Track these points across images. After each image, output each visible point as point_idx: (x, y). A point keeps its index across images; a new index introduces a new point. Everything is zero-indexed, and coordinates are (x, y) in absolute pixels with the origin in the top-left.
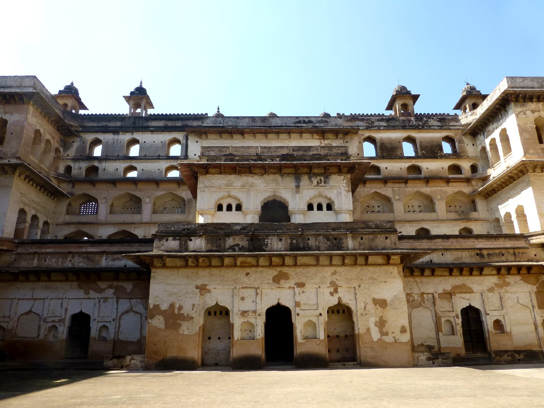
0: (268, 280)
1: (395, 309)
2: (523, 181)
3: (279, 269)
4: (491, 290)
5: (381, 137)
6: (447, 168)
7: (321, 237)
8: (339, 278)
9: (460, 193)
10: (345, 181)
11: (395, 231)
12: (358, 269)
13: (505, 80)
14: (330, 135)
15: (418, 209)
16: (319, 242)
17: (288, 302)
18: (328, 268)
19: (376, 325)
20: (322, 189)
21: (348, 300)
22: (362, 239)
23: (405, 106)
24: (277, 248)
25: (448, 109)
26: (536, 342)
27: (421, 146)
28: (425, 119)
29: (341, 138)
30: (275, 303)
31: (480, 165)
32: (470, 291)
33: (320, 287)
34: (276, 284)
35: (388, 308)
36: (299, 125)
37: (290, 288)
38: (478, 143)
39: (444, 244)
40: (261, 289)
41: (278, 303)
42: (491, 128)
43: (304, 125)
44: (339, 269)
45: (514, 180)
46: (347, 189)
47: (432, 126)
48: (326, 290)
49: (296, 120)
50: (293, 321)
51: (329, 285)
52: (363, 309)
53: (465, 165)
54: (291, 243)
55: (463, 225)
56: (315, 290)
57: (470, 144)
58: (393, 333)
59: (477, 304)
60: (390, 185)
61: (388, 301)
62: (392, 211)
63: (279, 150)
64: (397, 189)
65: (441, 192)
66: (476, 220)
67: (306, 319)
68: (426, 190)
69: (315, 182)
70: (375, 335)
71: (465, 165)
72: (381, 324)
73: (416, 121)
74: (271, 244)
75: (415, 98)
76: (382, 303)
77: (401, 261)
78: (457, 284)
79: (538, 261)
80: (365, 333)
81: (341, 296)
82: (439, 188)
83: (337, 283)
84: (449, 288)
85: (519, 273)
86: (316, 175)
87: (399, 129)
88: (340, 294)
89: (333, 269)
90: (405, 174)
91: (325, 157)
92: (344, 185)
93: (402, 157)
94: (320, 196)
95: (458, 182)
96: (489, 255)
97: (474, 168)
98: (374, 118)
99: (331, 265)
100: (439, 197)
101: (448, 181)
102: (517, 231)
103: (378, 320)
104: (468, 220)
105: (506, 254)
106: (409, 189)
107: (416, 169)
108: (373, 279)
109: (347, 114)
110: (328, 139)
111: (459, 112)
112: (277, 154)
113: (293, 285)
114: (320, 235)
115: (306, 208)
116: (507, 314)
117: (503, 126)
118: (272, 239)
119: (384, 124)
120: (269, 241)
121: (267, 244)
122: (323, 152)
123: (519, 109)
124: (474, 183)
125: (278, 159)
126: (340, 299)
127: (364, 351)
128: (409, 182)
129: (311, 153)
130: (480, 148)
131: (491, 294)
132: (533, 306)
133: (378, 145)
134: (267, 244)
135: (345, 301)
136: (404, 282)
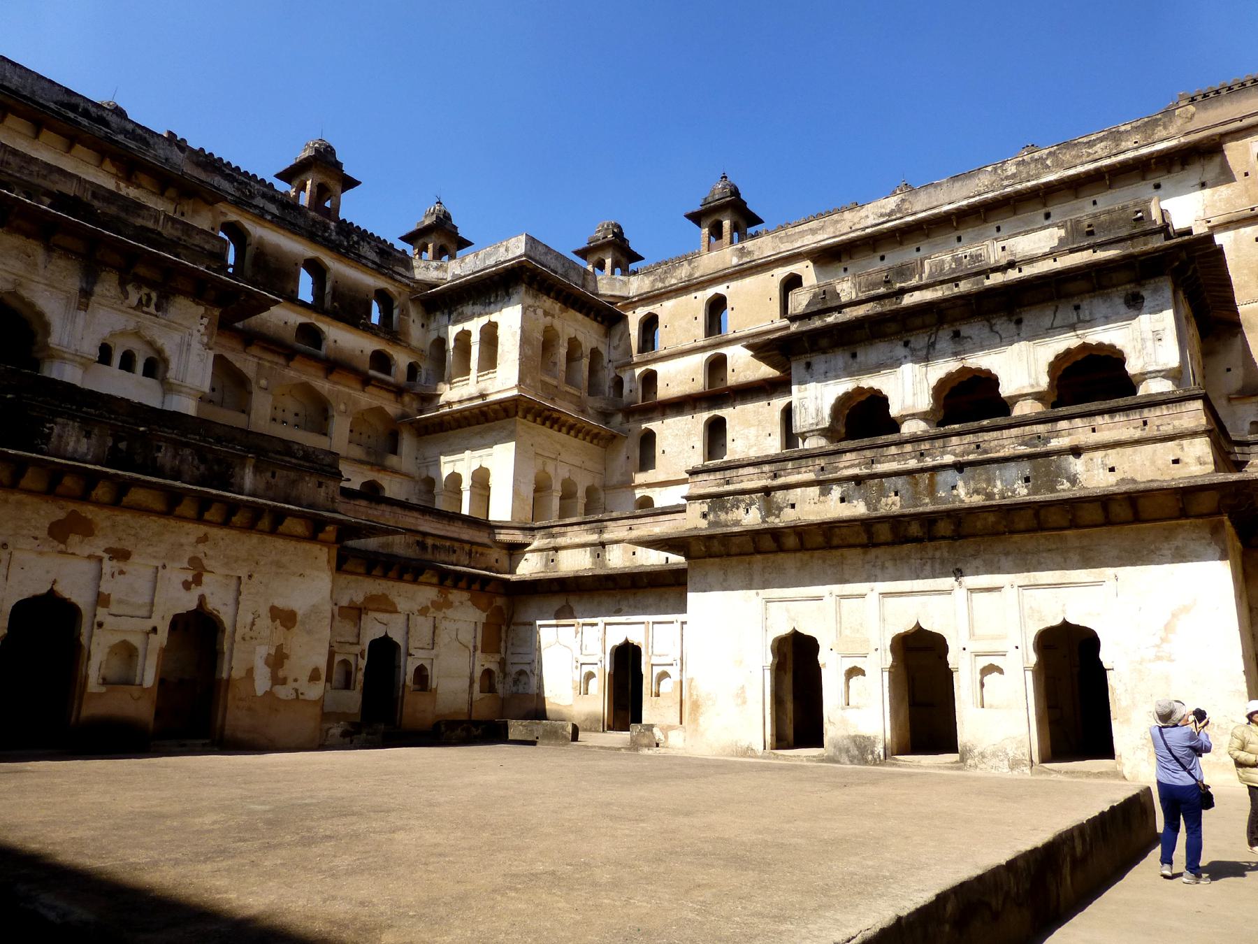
0: (36, 528)
1: (309, 632)
2: (503, 428)
3: (72, 506)
4: (423, 611)
5: (261, 237)
6: (369, 353)
7: (187, 451)
8: (210, 553)
9: (379, 411)
10: (205, 321)
11: (338, 476)
12: (254, 539)
13: (523, 238)
14: (144, 179)
15: (291, 418)
16: (182, 461)
17: (76, 589)
18: (191, 525)
19: (267, 663)
20: (146, 320)
21: (218, 599)
22: (273, 476)
23: (322, 192)
24: (75, 451)
25: (391, 231)
26: (466, 707)
27: (335, 289)
28: (355, 239)
29: (172, 200)
30: (43, 589)
31: (425, 368)
32: (393, 610)
33: (164, 567)
34: (56, 543)
35: (295, 630)
36: (72, 115)
37: (89, 557)
38: (433, 326)
39: (370, 512)
40: (10, 549)
41: (52, 592)
42: (468, 309)
43: (85, 122)
44: (215, 532)
45: (487, 421)
46: (205, 339)
47: (366, 258)
48: (176, 575)
49: (66, 99)
50: (84, 640)
51: (186, 565)
52: (248, 629)
53: (402, 360)
54: (114, 449)
55: (370, 475)
56: (150, 571)
57: (418, 323)
58: (296, 680)
59: (397, 637)
60: (255, 350)
61: (300, 613)
62: (245, 410)
63: (56, 177)
64: (267, 364)
65: (351, 401)
66: (395, 472)
67: (116, 639)
68: (324, 386)
69: (134, 298)
70: (262, 683)
71: (402, 360)
72: (278, 660)
73: (338, 234)
74: (60, 437)
75: (350, 183)
76: (286, 618)
77: (337, 538)
78: (374, 592)
79: (498, 572)
80: (242, 679)
81: (208, 595)
82: (347, 390)
83: (205, 562)
84: (359, 598)
85: (468, 588)
86: (140, 282)
87: (301, 235)
88: (204, 589)
89: (203, 529)
90: (290, 336)
91: (171, 245)
92: (202, 329)
93: (292, 299)
94: (137, 334)
95: (382, 388)
96: (435, 547)
97: (413, 370)
98: (257, 186)
99: (199, 519)
100: (342, 407)
101: (366, 381)
102: (465, 510)
103: (273, 652)
104: (383, 468)
105: (458, 552)
106: (292, 373)
107: (310, 334)
108: (278, 564)
109: (194, 144)
110: (139, 186)
111: (410, 250)
112: (46, 184)
113: (100, 553)
114: (187, 445)
115: (94, 353)
116: (437, 656)
117: (494, 317)
118: (64, 426)
119: (273, 208)
120: (56, 430)
121: (49, 436)
122: (168, 231)
123: (530, 301)
124: (407, 399)
125: (48, 201)
126: (202, 599)
127: (235, 717)
128: (298, 358)
129: (139, 222)
130: (433, 336)
131: (421, 619)
132: (475, 647)
133: (250, 251)
134: (50, 434)
135: (213, 604)
136: (333, 582)
